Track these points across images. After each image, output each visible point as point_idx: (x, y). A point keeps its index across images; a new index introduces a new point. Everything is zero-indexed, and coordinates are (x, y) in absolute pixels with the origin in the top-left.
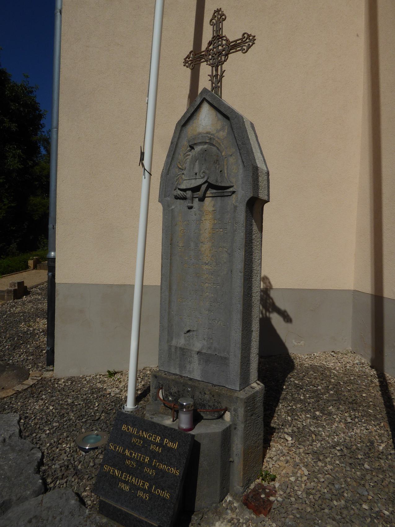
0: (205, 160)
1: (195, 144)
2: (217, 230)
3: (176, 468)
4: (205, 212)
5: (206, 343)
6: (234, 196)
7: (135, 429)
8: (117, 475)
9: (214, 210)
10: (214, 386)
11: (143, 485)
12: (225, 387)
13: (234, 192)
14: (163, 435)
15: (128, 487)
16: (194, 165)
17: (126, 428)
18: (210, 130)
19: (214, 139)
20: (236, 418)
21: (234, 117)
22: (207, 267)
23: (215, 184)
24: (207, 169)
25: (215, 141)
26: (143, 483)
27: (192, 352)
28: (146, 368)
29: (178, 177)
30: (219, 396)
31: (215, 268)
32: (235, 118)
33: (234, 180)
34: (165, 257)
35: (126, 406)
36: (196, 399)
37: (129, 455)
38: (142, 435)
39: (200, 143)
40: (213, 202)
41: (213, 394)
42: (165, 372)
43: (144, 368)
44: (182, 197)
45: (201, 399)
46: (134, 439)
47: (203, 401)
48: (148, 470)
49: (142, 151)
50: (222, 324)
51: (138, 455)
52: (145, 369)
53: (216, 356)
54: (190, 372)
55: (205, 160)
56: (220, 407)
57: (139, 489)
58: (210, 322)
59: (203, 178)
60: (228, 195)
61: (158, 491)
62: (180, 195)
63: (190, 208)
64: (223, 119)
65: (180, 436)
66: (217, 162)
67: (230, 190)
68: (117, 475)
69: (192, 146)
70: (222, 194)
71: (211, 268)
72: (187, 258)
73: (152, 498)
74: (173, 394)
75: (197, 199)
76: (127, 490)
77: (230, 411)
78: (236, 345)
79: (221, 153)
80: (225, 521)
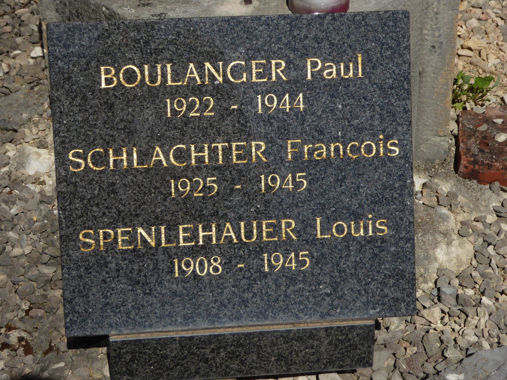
3: (381, 137)
7: (164, 68)
8: (153, 244)
14: (294, 50)
17: (117, 74)
38: (202, 77)
46: (172, 104)
48: (274, 179)
51: (213, 151)
68: (153, 244)
76: (216, 269)
80: (455, 237)
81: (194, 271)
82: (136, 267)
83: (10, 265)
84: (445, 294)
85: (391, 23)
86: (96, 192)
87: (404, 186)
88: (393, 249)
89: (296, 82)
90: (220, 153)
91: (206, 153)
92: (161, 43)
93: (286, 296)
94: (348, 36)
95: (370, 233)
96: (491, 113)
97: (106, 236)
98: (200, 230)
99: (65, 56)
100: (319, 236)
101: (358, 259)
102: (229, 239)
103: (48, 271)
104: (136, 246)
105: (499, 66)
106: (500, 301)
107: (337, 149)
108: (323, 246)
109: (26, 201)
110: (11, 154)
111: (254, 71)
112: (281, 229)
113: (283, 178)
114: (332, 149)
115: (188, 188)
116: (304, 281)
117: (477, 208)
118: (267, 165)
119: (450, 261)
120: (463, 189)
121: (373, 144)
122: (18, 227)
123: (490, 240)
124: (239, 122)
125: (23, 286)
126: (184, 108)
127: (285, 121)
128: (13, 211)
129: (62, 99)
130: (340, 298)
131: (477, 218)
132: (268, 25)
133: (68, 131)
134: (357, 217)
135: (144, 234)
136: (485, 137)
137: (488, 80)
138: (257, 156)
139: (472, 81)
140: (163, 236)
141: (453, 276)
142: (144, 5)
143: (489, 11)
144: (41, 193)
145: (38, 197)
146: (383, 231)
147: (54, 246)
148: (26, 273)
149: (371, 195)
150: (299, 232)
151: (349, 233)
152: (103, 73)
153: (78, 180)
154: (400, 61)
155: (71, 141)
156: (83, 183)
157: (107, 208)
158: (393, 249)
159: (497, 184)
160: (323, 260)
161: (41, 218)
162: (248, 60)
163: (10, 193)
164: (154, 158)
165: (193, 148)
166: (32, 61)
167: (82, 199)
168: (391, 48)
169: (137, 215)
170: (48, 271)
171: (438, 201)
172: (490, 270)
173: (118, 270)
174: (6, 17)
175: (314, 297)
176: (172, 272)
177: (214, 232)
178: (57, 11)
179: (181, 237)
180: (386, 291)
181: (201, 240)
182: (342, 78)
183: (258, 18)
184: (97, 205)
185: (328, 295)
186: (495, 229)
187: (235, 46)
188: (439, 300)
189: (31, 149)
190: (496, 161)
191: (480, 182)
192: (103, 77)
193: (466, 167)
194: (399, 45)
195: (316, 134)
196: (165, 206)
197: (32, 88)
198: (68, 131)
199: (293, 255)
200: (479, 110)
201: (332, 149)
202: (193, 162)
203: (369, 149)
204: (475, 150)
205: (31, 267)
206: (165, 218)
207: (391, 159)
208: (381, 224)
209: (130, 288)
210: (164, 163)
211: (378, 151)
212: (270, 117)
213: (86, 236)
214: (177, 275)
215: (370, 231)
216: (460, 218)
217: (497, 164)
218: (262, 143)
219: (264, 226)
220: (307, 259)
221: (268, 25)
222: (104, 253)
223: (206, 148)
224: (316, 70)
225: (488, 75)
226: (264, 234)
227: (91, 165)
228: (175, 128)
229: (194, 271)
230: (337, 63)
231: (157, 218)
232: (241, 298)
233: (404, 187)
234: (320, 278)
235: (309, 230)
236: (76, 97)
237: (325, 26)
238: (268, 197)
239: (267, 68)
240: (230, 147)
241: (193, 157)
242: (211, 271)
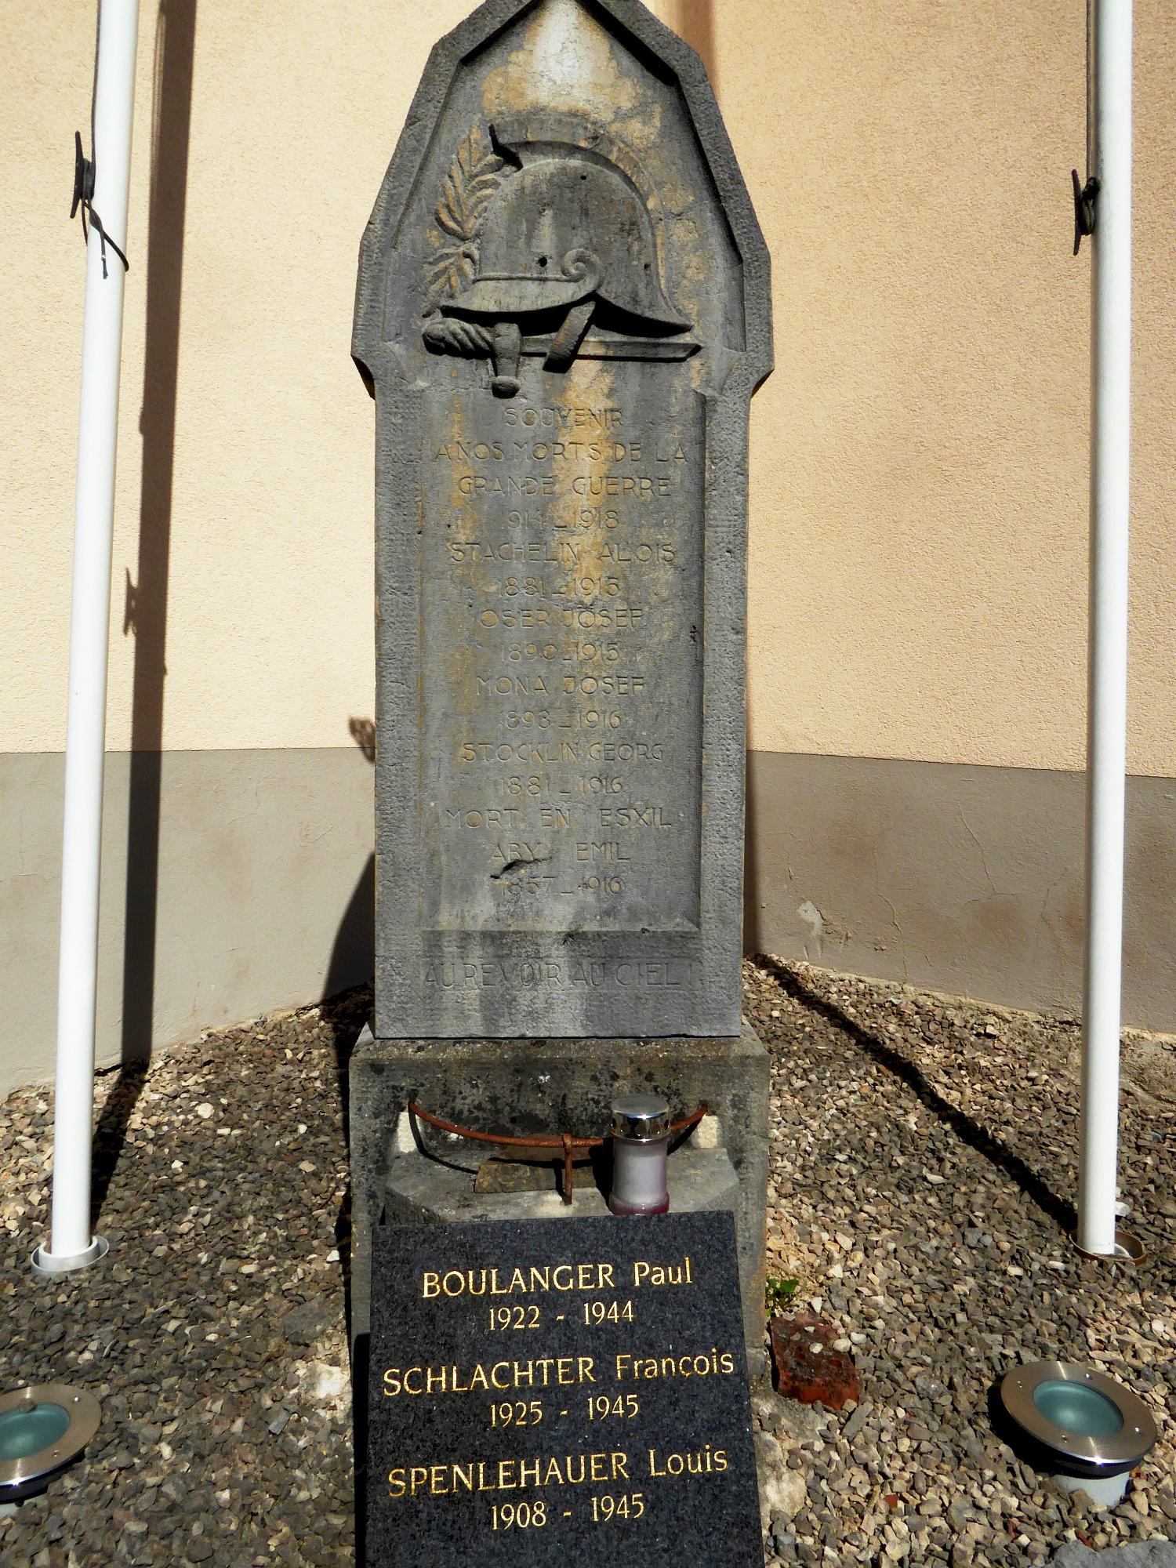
0: (585, 212)
1: (527, 145)
2: (629, 483)
3: (714, 1350)
4: (573, 413)
5: (591, 899)
6: (695, 363)
7: (489, 1275)
8: (470, 1486)
9: (612, 410)
10: (646, 1044)
11: (606, 1468)
12: (685, 1036)
13: (695, 350)
14: (621, 1253)
15: (539, 1507)
16: (533, 225)
17: (440, 1282)
18: (582, 105)
19: (612, 142)
20: (741, 1127)
21: (699, 77)
22: (586, 617)
23: (628, 308)
24: (595, 250)
25: (615, 149)
26: (598, 1461)
27: (540, 941)
28: (20, 1094)
29: (442, 265)
30: (675, 1070)
31: (624, 621)
32: (699, 82)
33: (692, 307)
34: (395, 585)
35: (49, 1249)
36: (576, 1108)
37: (496, 1384)
38: (527, 1284)
39: (549, 144)
40: (608, 379)
41: (646, 1071)
42: (412, 1039)
43: (10, 1095)
44: (470, 344)
45: (597, 1102)
46: (496, 1315)
47: (606, 1107)
48: (603, 1403)
49: (87, 156)
50: (657, 818)
51: (538, 1370)
52: (15, 1096)
53: (647, 934)
54: (533, 1015)
55: (585, 212)
56: (680, 1106)
57: (590, 1490)
58: (608, 818)
59: (575, 280)
60: (672, 356)
61: (675, 1461)
62: (462, 336)
63: (504, 392)
64: (644, 76)
65: (689, 1231)
66: (630, 228)
67: (682, 341)
68: (470, 1486)
69: (513, 150)
70: (650, 353)
71: (606, 621)
72: (493, 588)
73: (658, 1498)
74: (466, 1113)
75: (538, 363)
76: (539, 1520)
77: (718, 1112)
78: (723, 883)
79: (644, 199)
80: (784, 1469)
81: (515, 1521)
82: (450, 1517)
83: (294, 1513)
84: (782, 1543)
85: (716, 1225)
86: (411, 1421)
87: (741, 1408)
88: (734, 1488)
89: (624, 1288)
90: (545, 1371)
91: (530, 1372)
92: (487, 1247)
93: (618, 1553)
94: (675, 1238)
95: (709, 1469)
96: (802, 1321)
97: (419, 1476)
98: (523, 1467)
99: (389, 1262)
100: (653, 1473)
101: (697, 1503)
102: (554, 1478)
103: (337, 1521)
104: (451, 1489)
105: (801, 1268)
106: (844, 1552)
107: (669, 1365)
108: (658, 1487)
109: (316, 1430)
110: (301, 1373)
111: (581, 1277)
112: (611, 1465)
113: (613, 1401)
114: (664, 1366)
115: (510, 1415)
116: (638, 1533)
117: (802, 1433)
118: (596, 1385)
119: (782, 1501)
120: (786, 1411)
121: (706, 1360)
122: (306, 1464)
123: (822, 1473)
124: (565, 1335)
125: (309, 1541)
126: (509, 1319)
127: (614, 1333)
128: (302, 1443)
129: (382, 1309)
130: (679, 1554)
131: (1079, 1496)
132: (595, 1227)
133: (386, 1347)
134: (694, 1448)
135: (461, 1474)
136: (800, 1348)
137: (795, 1283)
138: (585, 1375)
139: (778, 1285)
140: (481, 1476)
141: (789, 1521)
142: (464, 1206)
143: (782, 1210)
144: (333, 1420)
145: (329, 1425)
146: (722, 1465)
147: (345, 1488)
148: (312, 1524)
149: (708, 1422)
150: (631, 1468)
151: (686, 1468)
152: (426, 1280)
153: (392, 1406)
154: (728, 1265)
155: (388, 1359)
156: (397, 1410)
157: (422, 1441)
158: (734, 1488)
159: (819, 1402)
160: (659, 1505)
161: (331, 1453)
162: (575, 1265)
163: (298, 1420)
164: (475, 1379)
165: (516, 1366)
166: (327, 1266)
167: (395, 1430)
168: (718, 1251)
169: (454, 1450)
170: (337, 1521)
171: (761, 1425)
172: (826, 1512)
173: (429, 1522)
174: (303, 1218)
175: (650, 1554)
176: (491, 1523)
177: (537, 1471)
178: (369, 1212)
179: (501, 1478)
180: (730, 1544)
181: (523, 1481)
182: (671, 1284)
183: (584, 1220)
184: (411, 1437)
185: (665, 1550)
186: (824, 1458)
187: (562, 1251)
188: (777, 1552)
189: (322, 1367)
190: (817, 1376)
191: (801, 1401)
192: (426, 1284)
193: (785, 1383)
194: (725, 1247)
195: (646, 1348)
196: (485, 1437)
197: (328, 1296)
198: (386, 1347)
199: (625, 1499)
200: (789, 1317)
201: (664, 1366)
202: (516, 1383)
203: (702, 1366)
204: (792, 1363)
205: (318, 1515)
206: (485, 1453)
207: (726, 1377)
208: (720, 1456)
209: (442, 1544)
210: (485, 1384)
211: (711, 1367)
212: (598, 1329)
213: (397, 1477)
214: (495, 1528)
215: (709, 1466)
216: (788, 1444)
217: (818, 1380)
218: (590, 1359)
219: (593, 1462)
220: (641, 1504)
221: (595, 1227)
222: (415, 1499)
223: (530, 1366)
224: (644, 1274)
225: (792, 1278)
226: (593, 1473)
227: (407, 1388)
228: (498, 1343)
229: (515, 1521)
230: (665, 1268)
231: (474, 1453)
232: (568, 1556)
233: (741, 1410)
234: (657, 1528)
235: (642, 1466)
236: (397, 1307)
237: (652, 1228)
238: (596, 1425)
239: (594, 1273)
240: (556, 1363)
241: (516, 1377)
242: (534, 1522)
